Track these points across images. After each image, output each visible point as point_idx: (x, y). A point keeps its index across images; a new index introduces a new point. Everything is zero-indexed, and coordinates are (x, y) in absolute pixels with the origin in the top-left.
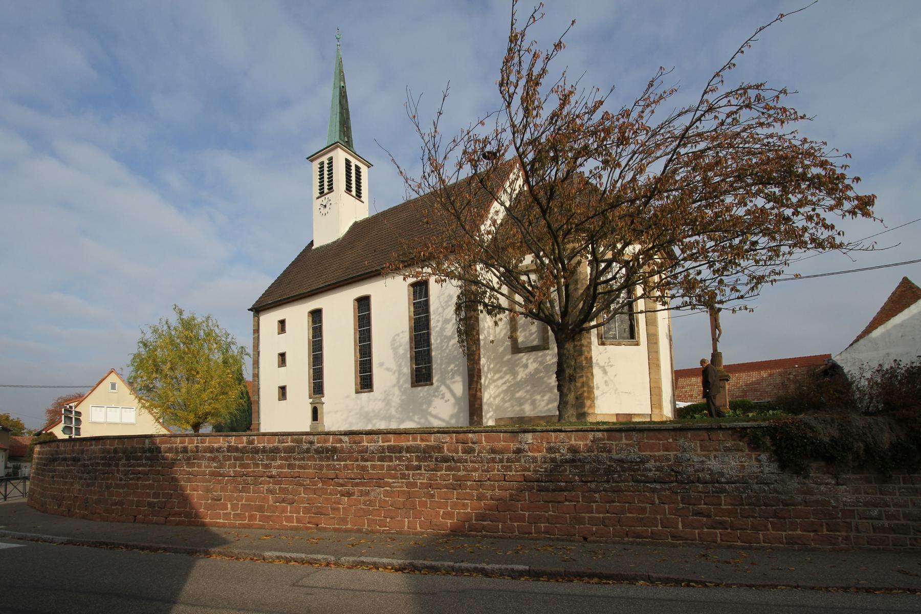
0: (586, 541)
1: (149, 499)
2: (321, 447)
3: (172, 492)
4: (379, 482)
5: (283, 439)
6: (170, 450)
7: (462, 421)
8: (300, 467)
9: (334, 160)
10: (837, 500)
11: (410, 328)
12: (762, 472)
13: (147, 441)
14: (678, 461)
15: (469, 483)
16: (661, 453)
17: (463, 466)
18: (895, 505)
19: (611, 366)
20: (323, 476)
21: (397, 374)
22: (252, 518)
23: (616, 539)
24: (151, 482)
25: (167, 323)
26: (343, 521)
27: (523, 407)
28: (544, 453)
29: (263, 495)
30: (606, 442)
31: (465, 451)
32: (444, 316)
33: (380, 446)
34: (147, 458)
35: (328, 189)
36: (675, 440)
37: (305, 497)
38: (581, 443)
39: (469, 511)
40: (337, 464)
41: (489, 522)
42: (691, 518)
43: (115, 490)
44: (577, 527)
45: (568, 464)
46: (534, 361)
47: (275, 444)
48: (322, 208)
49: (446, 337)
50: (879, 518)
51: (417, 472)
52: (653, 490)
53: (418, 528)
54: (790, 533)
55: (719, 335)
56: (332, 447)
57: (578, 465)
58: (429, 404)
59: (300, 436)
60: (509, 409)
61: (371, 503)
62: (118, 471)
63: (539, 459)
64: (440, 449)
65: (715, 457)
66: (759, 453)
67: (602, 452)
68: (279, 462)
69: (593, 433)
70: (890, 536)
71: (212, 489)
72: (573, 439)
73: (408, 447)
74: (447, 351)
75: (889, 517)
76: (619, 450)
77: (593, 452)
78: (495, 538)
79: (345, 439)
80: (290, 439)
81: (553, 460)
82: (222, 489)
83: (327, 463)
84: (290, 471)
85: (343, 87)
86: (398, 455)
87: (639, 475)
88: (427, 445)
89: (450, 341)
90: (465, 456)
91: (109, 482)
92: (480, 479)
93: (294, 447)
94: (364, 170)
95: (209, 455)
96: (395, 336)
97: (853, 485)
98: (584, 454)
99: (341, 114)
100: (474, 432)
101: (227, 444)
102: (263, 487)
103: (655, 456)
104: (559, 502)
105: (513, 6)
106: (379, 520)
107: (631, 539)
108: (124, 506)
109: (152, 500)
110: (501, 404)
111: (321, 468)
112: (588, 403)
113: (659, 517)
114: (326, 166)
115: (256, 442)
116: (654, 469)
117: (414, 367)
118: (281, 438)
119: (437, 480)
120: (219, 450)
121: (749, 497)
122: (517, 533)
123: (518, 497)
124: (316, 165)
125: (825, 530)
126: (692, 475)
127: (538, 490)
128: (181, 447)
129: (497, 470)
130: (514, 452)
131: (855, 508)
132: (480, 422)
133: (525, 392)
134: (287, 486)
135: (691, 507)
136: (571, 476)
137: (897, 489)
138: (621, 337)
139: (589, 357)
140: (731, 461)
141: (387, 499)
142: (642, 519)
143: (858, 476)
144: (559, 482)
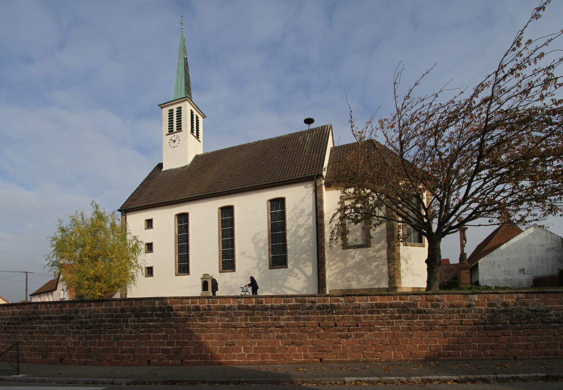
0: (516, 359)
1: (162, 347)
2: (322, 305)
3: (187, 340)
4: (370, 327)
5: (289, 300)
6: (182, 309)
7: (313, 290)
8: (305, 319)
9: (182, 109)
11: (268, 230)
13: (157, 302)
16: (558, 306)
17: (432, 316)
19: (410, 259)
20: (325, 325)
21: (257, 260)
22: (263, 357)
23: (534, 356)
24: (164, 333)
25: (82, 214)
26: (344, 355)
27: (350, 283)
28: (486, 307)
29: (273, 340)
30: (525, 299)
31: (433, 306)
32: (298, 223)
33: (370, 304)
34: (157, 315)
35: (177, 129)
37: (310, 341)
38: (510, 300)
39: (438, 344)
40: (336, 317)
41: (453, 351)
43: (125, 341)
44: (510, 351)
45: (502, 313)
46: (360, 254)
47: (281, 304)
48: (171, 142)
49: (299, 236)
51: (399, 320)
52: (555, 328)
53: (402, 357)
55: (465, 243)
56: (330, 305)
57: (508, 314)
58: (285, 280)
59: (304, 298)
60: (341, 284)
62: (127, 326)
63: (484, 310)
64: (415, 305)
67: (523, 306)
68: (286, 316)
69: (516, 294)
71: (226, 337)
72: (504, 298)
73: (391, 304)
74: (300, 246)
76: (533, 304)
77: (517, 306)
78: (457, 360)
79: (342, 299)
80: (294, 300)
81: (493, 311)
82: (235, 337)
83: (327, 316)
84: (296, 322)
85: (186, 58)
86: (384, 309)
87: (546, 319)
88: (405, 303)
89: (303, 239)
90: (433, 309)
91: (119, 334)
92: (445, 324)
93: (299, 305)
94: (201, 119)
95: (221, 312)
96: (256, 234)
98: (512, 307)
99: (186, 78)
101: (237, 304)
102: (273, 335)
103: (554, 307)
105: (529, 22)
107: (543, 357)
108: (136, 353)
109: (166, 347)
110: (334, 281)
111: (323, 319)
112: (398, 281)
113: (559, 343)
115: (264, 302)
116: (554, 315)
117: (271, 255)
118: (286, 299)
119: (415, 325)
120: (230, 308)
122: (472, 357)
123: (471, 334)
124: (166, 111)
128: (193, 307)
129: (455, 319)
130: (467, 306)
132: (256, 294)
133: (353, 274)
134: (294, 333)
136: (504, 320)
138: (414, 241)
141: (378, 339)
142: (549, 344)
144: (497, 324)
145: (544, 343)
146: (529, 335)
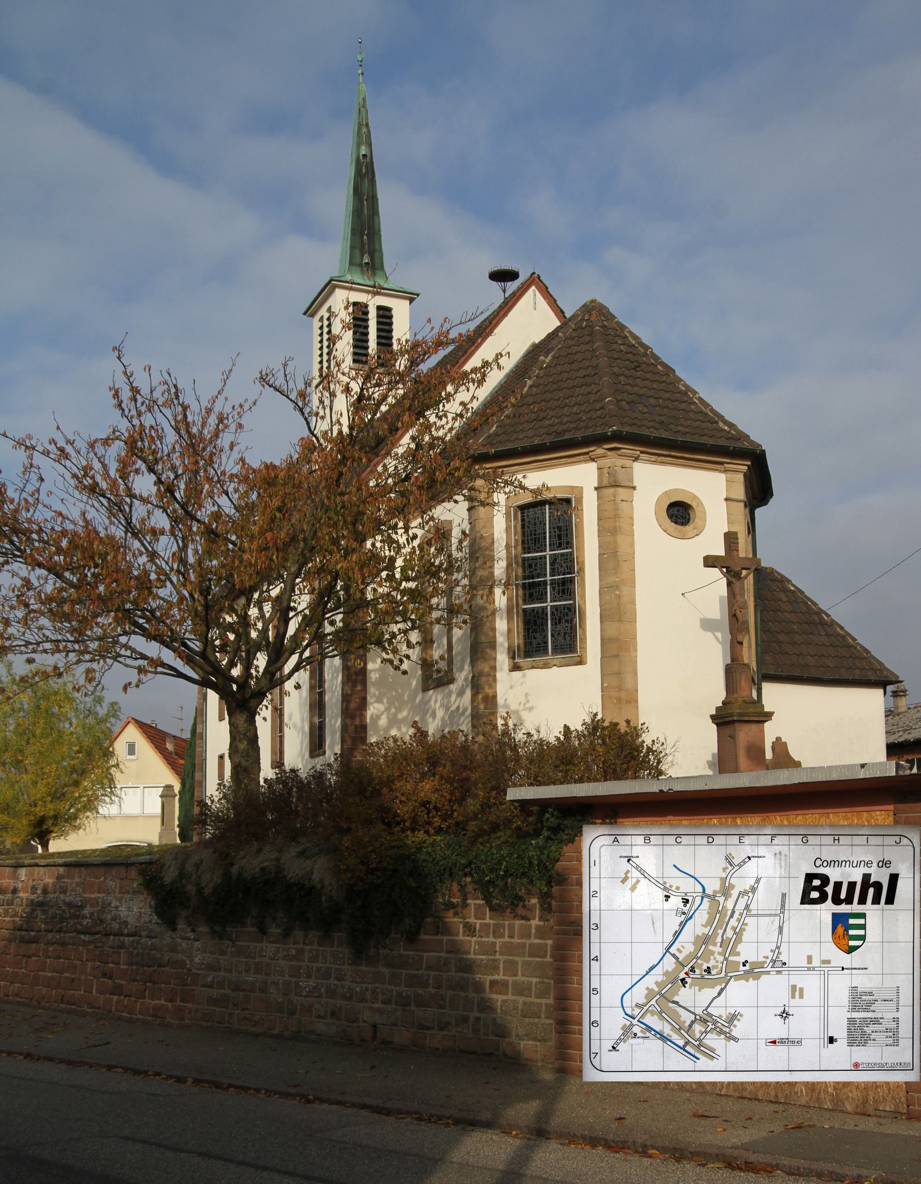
19: (531, 709)
30: (65, 880)
52: (85, 944)
85: (364, 156)
99: (357, 212)
103: (90, 899)
139: (491, 694)
142: (73, 980)
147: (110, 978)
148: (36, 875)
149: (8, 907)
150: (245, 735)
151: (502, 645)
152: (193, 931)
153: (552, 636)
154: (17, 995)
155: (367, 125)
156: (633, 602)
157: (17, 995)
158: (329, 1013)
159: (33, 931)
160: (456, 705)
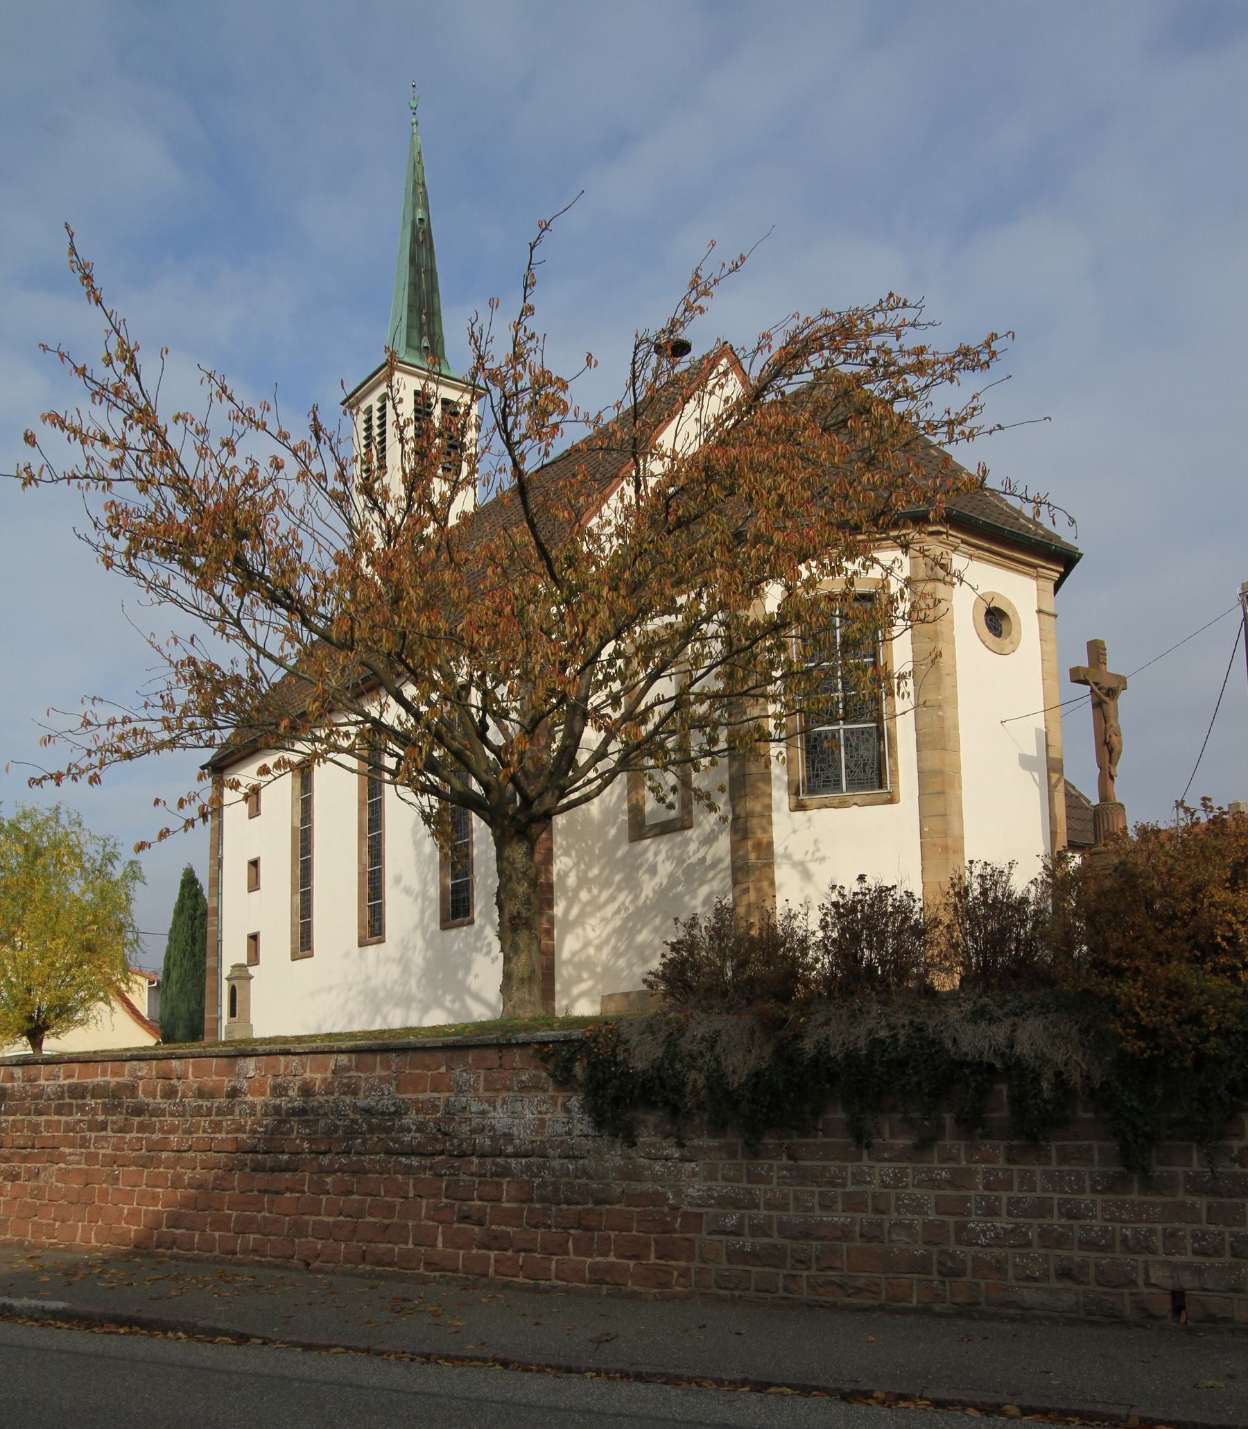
4: (51, 1152)
10: (678, 1193)
12: (569, 1133)
14: (450, 1115)
15: (164, 1155)
18: (769, 1205)
19: (823, 859)
21: (419, 901)
30: (353, 1073)
36: (450, 1068)
41: (183, 1231)
42: (456, 1226)
50: (736, 1232)
52: (408, 1171)
54: (598, 1259)
61: (38, 1193)
64: (131, 1089)
65: (504, 1102)
66: (569, 1094)
70: (753, 1269)
75: (757, 1230)
77: (332, 1094)
79: (18, 1072)
81: (277, 1109)
85: (421, 220)
97: (708, 1161)
99: (414, 286)
100: (179, 1057)
103: (416, 1102)
104: (277, 1193)
106: (47, 1225)
107: (368, 1268)
110: (611, 962)
114: (376, 414)
117: (449, 882)
121: (543, 1185)
122: (217, 1252)
125: (653, 1255)
126: (465, 1140)
127: (254, 1170)
131: (705, 1210)
135: (457, 1204)
137: (775, 1169)
139: (765, 841)
140: (527, 1112)
142: (387, 1227)
143: (714, 1143)
145: (375, 1223)
146: (342, 1194)
147: (480, 1223)
148: (282, 1068)
149: (219, 1118)
150: (524, 873)
151: (778, 778)
152: (681, 1145)
153: (847, 767)
154: (254, 1251)
155: (423, 184)
156: (956, 727)
157: (254, 1251)
158: (1052, 1272)
159: (283, 1152)
160: (700, 855)
